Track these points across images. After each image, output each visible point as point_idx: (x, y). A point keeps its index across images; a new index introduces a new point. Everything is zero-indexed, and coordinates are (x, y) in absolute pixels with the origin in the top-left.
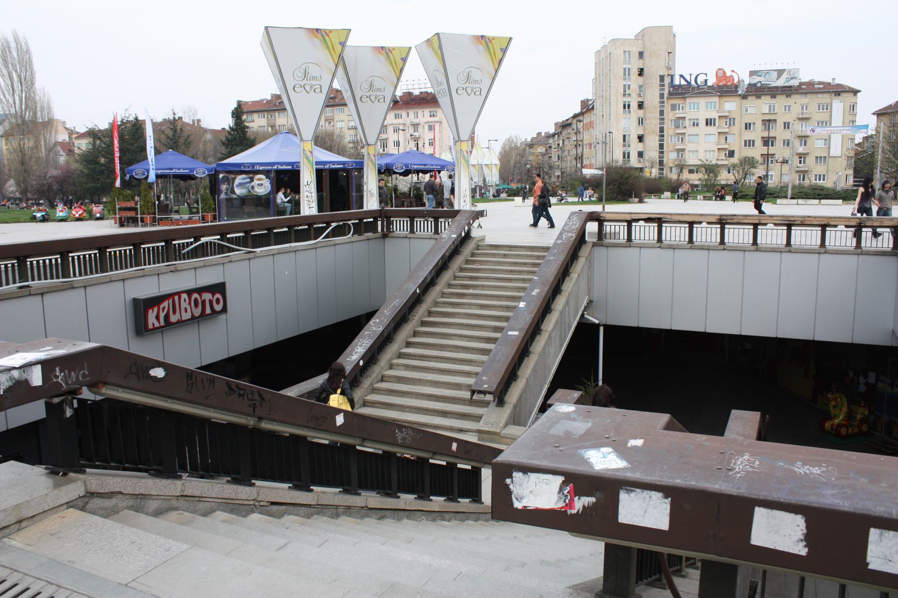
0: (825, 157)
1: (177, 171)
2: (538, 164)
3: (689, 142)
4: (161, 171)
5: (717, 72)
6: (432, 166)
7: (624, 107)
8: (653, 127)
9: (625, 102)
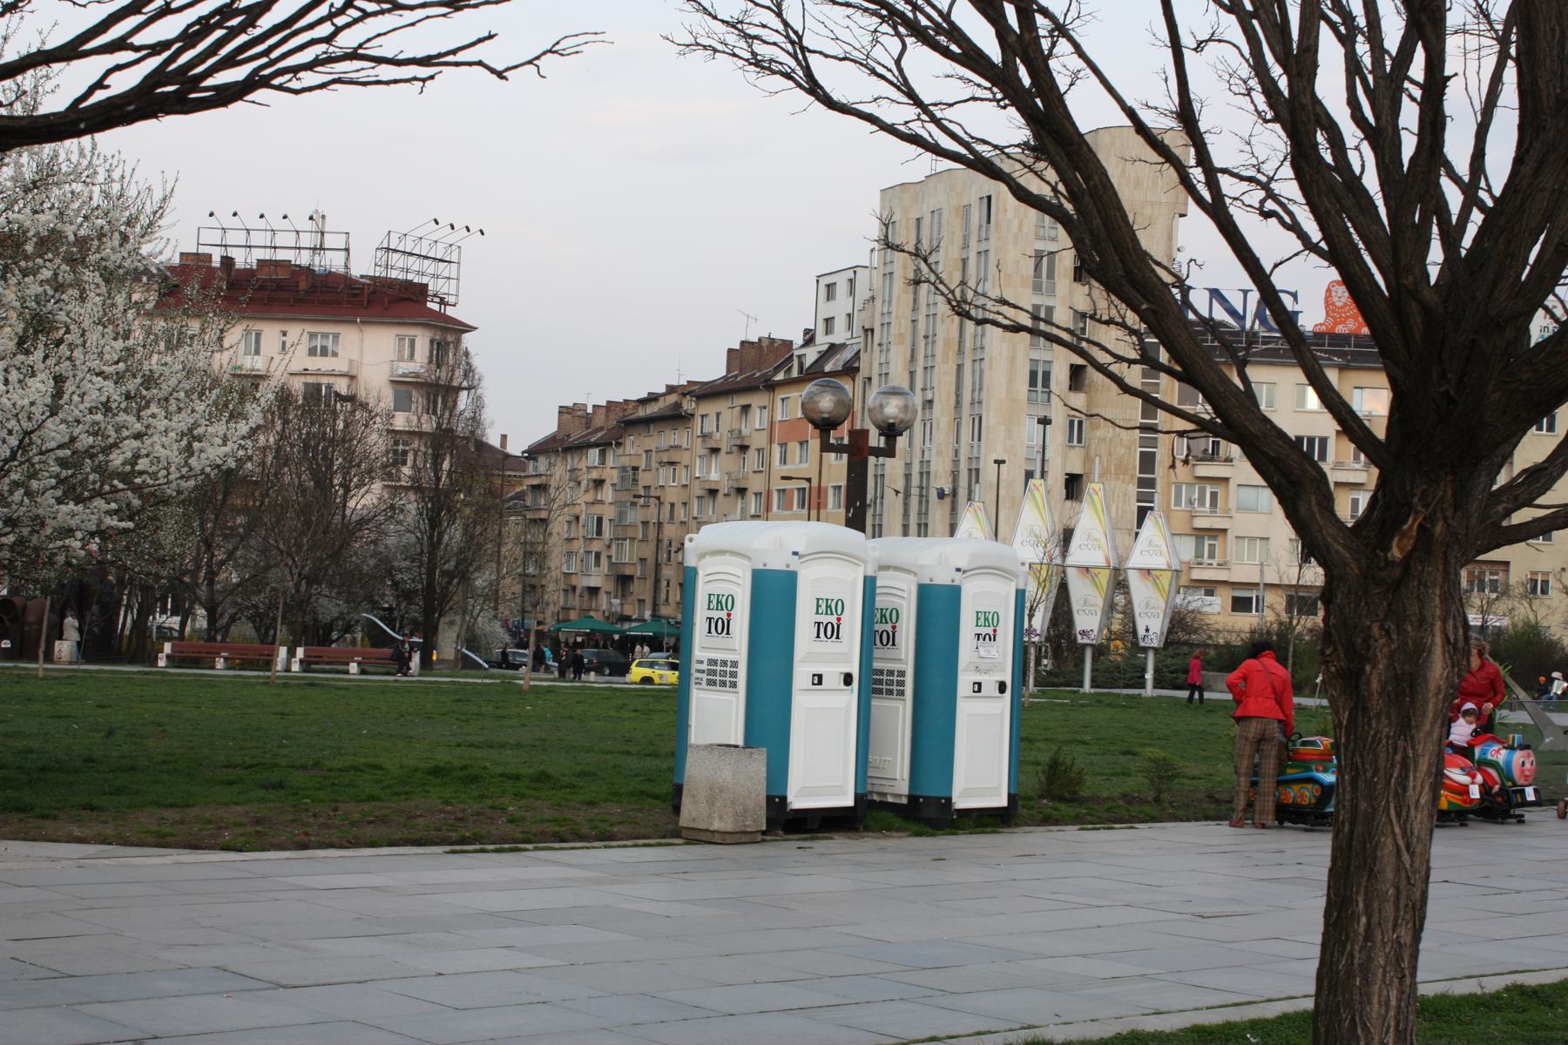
5: (1329, 290)
8: (1123, 451)
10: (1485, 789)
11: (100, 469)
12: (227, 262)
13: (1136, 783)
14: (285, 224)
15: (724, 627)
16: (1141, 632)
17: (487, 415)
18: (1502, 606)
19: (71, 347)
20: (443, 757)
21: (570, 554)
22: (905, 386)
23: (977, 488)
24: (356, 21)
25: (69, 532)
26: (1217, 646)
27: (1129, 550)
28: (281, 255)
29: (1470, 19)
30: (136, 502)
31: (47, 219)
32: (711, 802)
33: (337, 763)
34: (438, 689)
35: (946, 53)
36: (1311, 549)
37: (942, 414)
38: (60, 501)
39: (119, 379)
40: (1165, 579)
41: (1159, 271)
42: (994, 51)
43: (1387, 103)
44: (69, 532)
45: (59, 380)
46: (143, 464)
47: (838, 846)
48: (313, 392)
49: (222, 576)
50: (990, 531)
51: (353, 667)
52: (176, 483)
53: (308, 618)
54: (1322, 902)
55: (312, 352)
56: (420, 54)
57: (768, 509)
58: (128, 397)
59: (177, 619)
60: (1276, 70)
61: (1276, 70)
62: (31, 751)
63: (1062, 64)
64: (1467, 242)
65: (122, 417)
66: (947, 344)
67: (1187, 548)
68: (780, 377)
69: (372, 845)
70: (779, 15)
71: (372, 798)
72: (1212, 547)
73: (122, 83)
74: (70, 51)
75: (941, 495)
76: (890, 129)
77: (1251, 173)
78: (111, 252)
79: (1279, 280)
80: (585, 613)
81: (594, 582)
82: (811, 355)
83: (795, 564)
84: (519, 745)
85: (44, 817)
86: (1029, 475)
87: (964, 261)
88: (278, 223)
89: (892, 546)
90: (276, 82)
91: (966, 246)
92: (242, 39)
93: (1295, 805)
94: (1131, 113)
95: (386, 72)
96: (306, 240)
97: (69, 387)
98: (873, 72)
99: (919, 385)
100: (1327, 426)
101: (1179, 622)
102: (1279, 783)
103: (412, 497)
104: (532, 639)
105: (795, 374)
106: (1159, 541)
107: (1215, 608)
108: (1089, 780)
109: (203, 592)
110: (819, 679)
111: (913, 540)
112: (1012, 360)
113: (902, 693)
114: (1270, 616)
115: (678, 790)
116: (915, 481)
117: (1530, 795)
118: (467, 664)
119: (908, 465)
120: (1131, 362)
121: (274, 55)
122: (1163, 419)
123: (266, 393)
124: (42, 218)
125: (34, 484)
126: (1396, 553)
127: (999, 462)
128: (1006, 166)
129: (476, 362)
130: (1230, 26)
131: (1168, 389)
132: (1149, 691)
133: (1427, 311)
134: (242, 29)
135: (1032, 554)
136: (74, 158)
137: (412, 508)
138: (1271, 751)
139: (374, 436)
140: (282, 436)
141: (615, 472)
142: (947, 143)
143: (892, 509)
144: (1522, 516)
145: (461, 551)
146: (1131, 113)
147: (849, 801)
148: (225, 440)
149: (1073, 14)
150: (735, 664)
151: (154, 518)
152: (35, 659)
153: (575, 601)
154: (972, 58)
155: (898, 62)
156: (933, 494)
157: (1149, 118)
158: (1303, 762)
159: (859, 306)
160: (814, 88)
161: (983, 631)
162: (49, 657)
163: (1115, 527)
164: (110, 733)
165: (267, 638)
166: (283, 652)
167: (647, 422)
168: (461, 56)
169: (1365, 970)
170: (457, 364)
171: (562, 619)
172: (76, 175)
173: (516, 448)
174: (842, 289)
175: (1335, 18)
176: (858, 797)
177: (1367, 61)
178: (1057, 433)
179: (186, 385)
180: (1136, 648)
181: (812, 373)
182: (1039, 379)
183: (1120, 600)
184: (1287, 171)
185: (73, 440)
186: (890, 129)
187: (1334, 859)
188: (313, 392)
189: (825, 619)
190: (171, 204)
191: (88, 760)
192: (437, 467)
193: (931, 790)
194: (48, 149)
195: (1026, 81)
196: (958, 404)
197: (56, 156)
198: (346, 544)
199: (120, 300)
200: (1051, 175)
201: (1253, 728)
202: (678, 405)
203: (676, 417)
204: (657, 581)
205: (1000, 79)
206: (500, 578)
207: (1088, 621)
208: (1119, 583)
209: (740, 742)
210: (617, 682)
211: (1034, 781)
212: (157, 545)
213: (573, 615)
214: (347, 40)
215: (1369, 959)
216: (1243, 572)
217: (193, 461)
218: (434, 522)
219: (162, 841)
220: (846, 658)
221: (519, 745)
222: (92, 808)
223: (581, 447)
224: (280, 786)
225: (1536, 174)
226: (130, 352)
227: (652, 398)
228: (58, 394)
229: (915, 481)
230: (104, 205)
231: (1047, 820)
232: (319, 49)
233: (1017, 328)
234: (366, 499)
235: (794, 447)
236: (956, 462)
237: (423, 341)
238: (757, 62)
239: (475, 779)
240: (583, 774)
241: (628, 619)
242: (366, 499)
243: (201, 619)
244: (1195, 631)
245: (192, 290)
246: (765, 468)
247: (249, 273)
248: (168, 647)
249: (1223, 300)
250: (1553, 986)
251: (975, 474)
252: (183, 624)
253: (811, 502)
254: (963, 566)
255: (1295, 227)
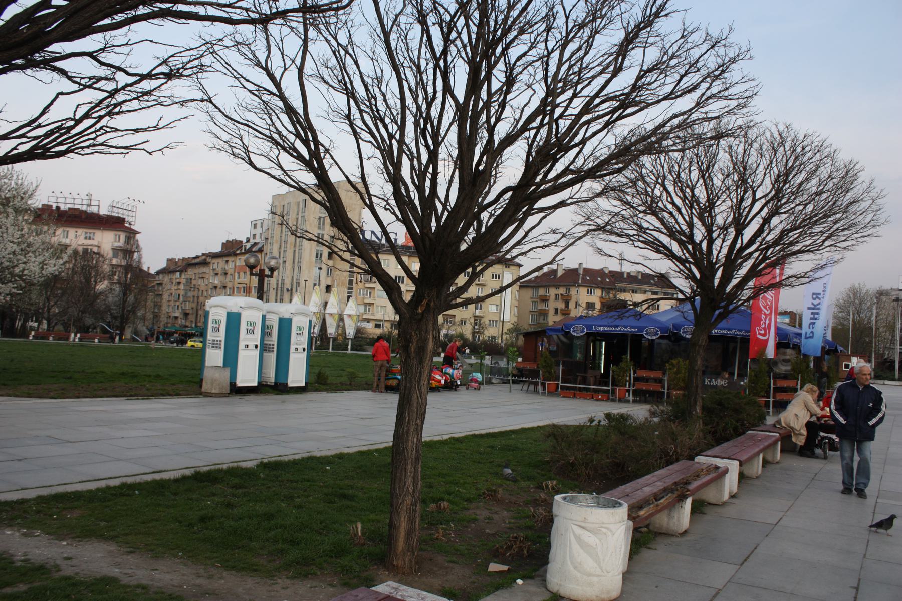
0: (496, 321)
1: (623, 329)
2: (580, 564)
4: (604, 328)
7: (317, 257)
9: (317, 250)
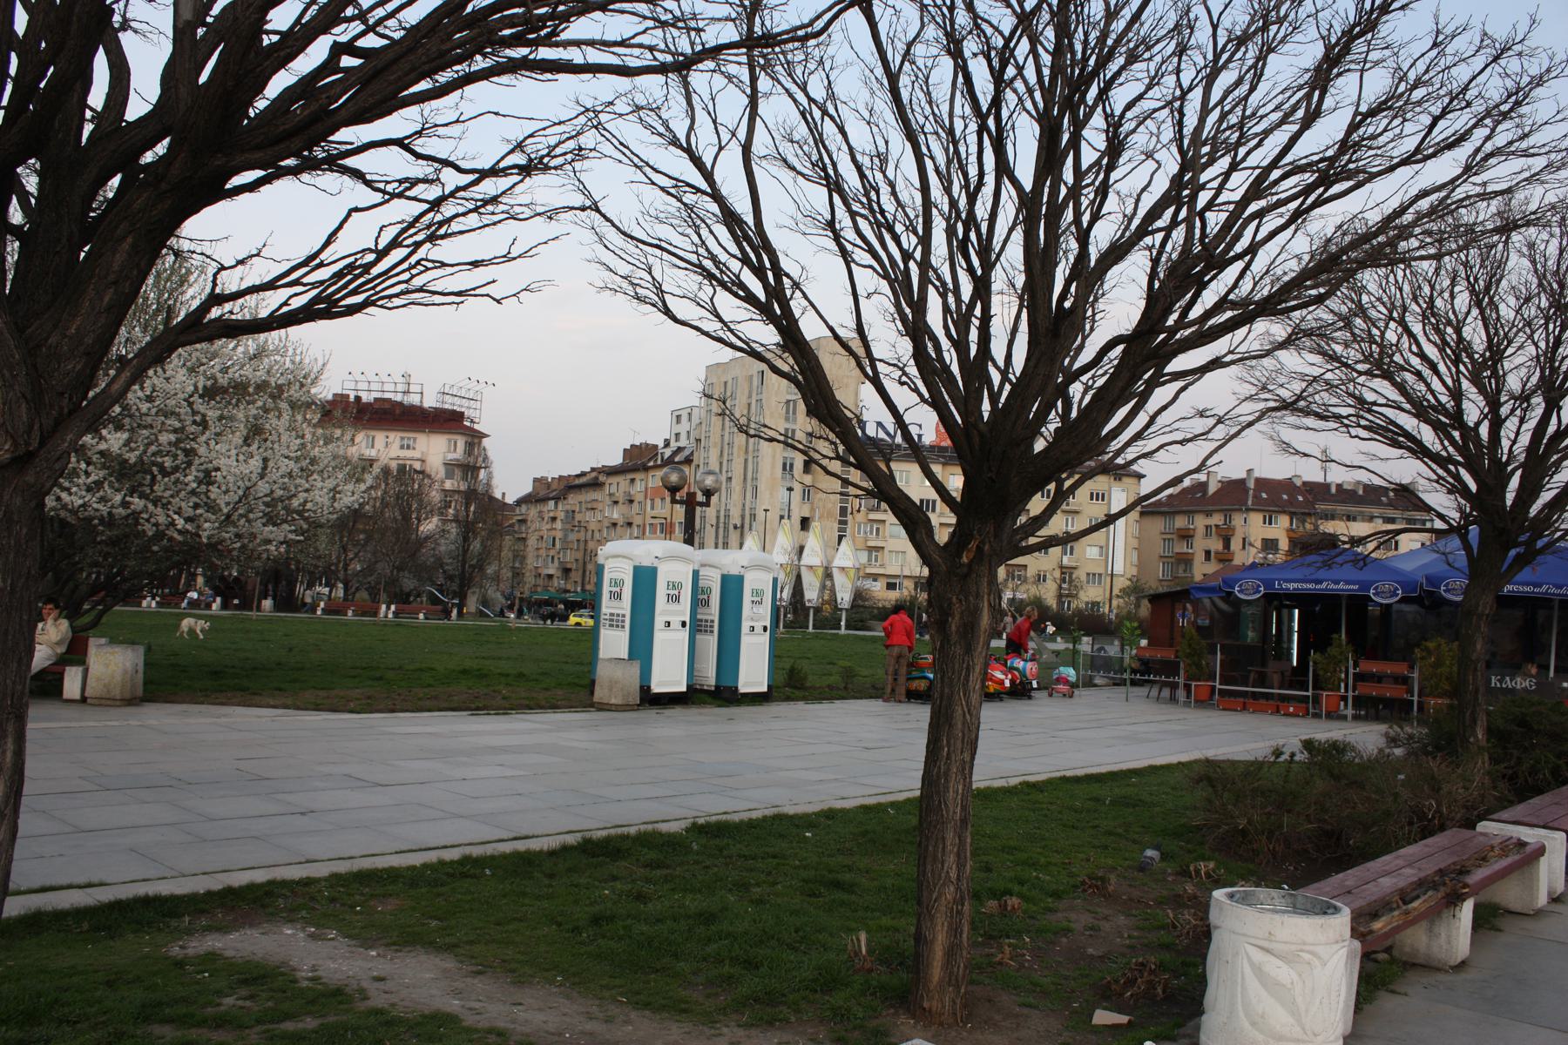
0: (1100, 575)
2: (1262, 1017)
3: (891, 536)
6: (1337, 582)
9: (785, 458)
10: (1012, 682)
11: (286, 508)
12: (358, 398)
13: (835, 679)
14: (390, 379)
15: (619, 596)
16: (839, 600)
17: (495, 482)
18: (1023, 588)
19: (273, 443)
20: (468, 664)
21: (538, 556)
22: (717, 470)
23: (754, 524)
24: (422, 272)
25: (269, 542)
26: (878, 608)
27: (833, 557)
28: (387, 396)
29: (1005, 287)
30: (305, 526)
31: (261, 375)
32: (611, 689)
33: (411, 667)
34: (466, 628)
35: (736, 295)
36: (926, 559)
37: (736, 484)
38: (264, 525)
39: (297, 460)
40: (852, 573)
41: (846, 412)
42: (762, 296)
43: (963, 328)
44: (269, 542)
45: (265, 460)
46: (309, 506)
47: (677, 712)
48: (402, 469)
49: (352, 566)
50: (760, 546)
51: (421, 616)
52: (327, 516)
53: (398, 590)
54: (926, 741)
55: (402, 447)
56: (456, 290)
57: (644, 533)
58: (302, 470)
59: (327, 589)
60: (908, 311)
61: (908, 311)
62: (247, 659)
63: (797, 304)
64: (1003, 400)
65: (298, 481)
66: (739, 447)
67: (863, 557)
68: (651, 464)
69: (429, 711)
70: (650, 273)
71: (429, 686)
72: (876, 556)
73: (297, 303)
74: (271, 285)
75: (735, 527)
76: (707, 334)
77: (895, 362)
78: (294, 392)
79: (907, 419)
80: (546, 588)
81: (551, 572)
82: (668, 453)
83: (656, 563)
84: (509, 658)
85: (255, 694)
86: (782, 517)
87: (749, 405)
88: (386, 379)
89: (710, 554)
90: (379, 303)
91: (750, 397)
92: (362, 280)
93: (916, 690)
94: (831, 329)
95: (438, 299)
96: (400, 388)
97: (271, 464)
98: (699, 304)
99: (724, 469)
100: (932, 494)
101: (859, 596)
102: (908, 679)
103: (454, 525)
104: (517, 601)
105: (659, 462)
106: (849, 553)
107: (878, 589)
108: (810, 678)
109: (341, 575)
110: (668, 624)
111: (720, 551)
112: (774, 457)
113: (712, 632)
114: (905, 592)
115: (593, 683)
116: (722, 520)
117: (1035, 685)
118: (482, 614)
119: (718, 511)
120: (831, 459)
121: (378, 289)
122: (852, 490)
123: (376, 470)
124: (258, 373)
125: (251, 516)
126: (965, 560)
127: (766, 510)
128: (769, 356)
129: (490, 454)
130: (884, 286)
131: (855, 475)
132: (843, 631)
133: (982, 435)
134: (361, 275)
135: (784, 559)
136: (276, 342)
137: (454, 530)
138: (904, 662)
139: (434, 493)
140: (385, 492)
141: (563, 514)
142: (740, 344)
143: (710, 534)
144: (1032, 540)
145: (480, 554)
146: (831, 329)
147: (684, 689)
148: (353, 493)
149: (804, 277)
150: (624, 616)
151: (315, 535)
152: (251, 610)
153: (540, 582)
154: (750, 298)
155: (711, 300)
156: (731, 527)
157: (841, 332)
158: (920, 668)
159: (693, 426)
160: (667, 312)
161: (755, 599)
162: (259, 608)
163: (826, 545)
164: (291, 650)
165: (376, 601)
166: (384, 607)
167: (580, 487)
168: (478, 292)
169: (947, 774)
170: (479, 455)
171: (533, 591)
172: (277, 351)
173: (510, 500)
174: (684, 418)
175: (938, 284)
176: (689, 687)
177: (953, 307)
178: (797, 495)
179: (333, 464)
180: (836, 609)
181: (669, 462)
182: (787, 467)
183: (828, 583)
184: (912, 362)
185: (272, 492)
186: (707, 334)
187: (932, 718)
188: (402, 469)
189: (672, 592)
190: (328, 367)
191: (279, 664)
192: (467, 510)
193: (727, 683)
194: (262, 336)
195: (778, 312)
196: (745, 479)
197: (266, 341)
198: (418, 550)
199: (299, 418)
200: (791, 361)
201: (896, 650)
202: (597, 478)
203: (595, 485)
204: (584, 571)
205: (764, 310)
206: (500, 569)
207: (811, 595)
208: (828, 575)
209: (626, 657)
210: (562, 625)
211: (781, 678)
212: (317, 550)
213: (539, 589)
214: (418, 282)
215: (949, 770)
216: (893, 570)
217: (336, 505)
218: (466, 539)
219: (317, 708)
220: (683, 613)
221: (509, 658)
222: (280, 690)
223: (545, 500)
224: (380, 679)
225: (1036, 367)
226: (303, 446)
227: (583, 474)
228: (265, 468)
229: (722, 520)
230: (291, 366)
231: (788, 699)
232: (403, 286)
233: (772, 440)
234: (429, 526)
235: (658, 501)
236: (743, 510)
237: (461, 442)
238: (638, 298)
239: (486, 676)
240: (543, 674)
241: (569, 591)
242: (429, 526)
243: (340, 592)
244: (867, 600)
245: (337, 413)
246: (643, 513)
247: (369, 404)
248: (322, 604)
249: (884, 428)
250: (1043, 782)
251: (753, 516)
252: (331, 592)
253: (667, 530)
254: (745, 564)
255: (916, 390)
